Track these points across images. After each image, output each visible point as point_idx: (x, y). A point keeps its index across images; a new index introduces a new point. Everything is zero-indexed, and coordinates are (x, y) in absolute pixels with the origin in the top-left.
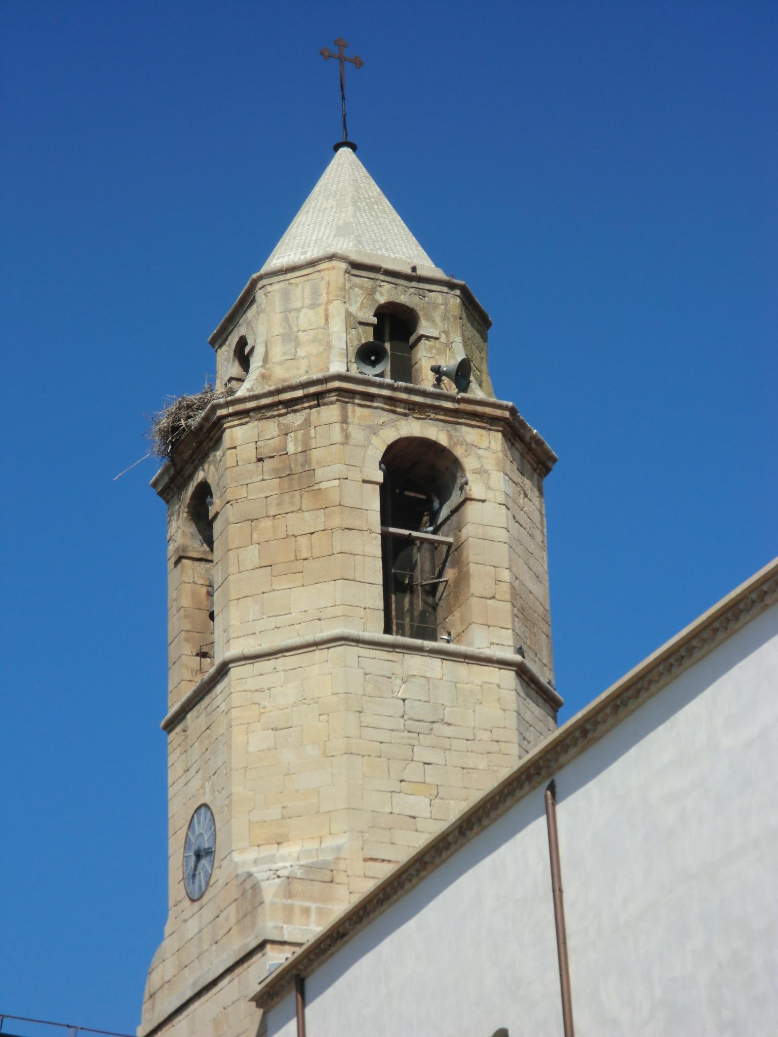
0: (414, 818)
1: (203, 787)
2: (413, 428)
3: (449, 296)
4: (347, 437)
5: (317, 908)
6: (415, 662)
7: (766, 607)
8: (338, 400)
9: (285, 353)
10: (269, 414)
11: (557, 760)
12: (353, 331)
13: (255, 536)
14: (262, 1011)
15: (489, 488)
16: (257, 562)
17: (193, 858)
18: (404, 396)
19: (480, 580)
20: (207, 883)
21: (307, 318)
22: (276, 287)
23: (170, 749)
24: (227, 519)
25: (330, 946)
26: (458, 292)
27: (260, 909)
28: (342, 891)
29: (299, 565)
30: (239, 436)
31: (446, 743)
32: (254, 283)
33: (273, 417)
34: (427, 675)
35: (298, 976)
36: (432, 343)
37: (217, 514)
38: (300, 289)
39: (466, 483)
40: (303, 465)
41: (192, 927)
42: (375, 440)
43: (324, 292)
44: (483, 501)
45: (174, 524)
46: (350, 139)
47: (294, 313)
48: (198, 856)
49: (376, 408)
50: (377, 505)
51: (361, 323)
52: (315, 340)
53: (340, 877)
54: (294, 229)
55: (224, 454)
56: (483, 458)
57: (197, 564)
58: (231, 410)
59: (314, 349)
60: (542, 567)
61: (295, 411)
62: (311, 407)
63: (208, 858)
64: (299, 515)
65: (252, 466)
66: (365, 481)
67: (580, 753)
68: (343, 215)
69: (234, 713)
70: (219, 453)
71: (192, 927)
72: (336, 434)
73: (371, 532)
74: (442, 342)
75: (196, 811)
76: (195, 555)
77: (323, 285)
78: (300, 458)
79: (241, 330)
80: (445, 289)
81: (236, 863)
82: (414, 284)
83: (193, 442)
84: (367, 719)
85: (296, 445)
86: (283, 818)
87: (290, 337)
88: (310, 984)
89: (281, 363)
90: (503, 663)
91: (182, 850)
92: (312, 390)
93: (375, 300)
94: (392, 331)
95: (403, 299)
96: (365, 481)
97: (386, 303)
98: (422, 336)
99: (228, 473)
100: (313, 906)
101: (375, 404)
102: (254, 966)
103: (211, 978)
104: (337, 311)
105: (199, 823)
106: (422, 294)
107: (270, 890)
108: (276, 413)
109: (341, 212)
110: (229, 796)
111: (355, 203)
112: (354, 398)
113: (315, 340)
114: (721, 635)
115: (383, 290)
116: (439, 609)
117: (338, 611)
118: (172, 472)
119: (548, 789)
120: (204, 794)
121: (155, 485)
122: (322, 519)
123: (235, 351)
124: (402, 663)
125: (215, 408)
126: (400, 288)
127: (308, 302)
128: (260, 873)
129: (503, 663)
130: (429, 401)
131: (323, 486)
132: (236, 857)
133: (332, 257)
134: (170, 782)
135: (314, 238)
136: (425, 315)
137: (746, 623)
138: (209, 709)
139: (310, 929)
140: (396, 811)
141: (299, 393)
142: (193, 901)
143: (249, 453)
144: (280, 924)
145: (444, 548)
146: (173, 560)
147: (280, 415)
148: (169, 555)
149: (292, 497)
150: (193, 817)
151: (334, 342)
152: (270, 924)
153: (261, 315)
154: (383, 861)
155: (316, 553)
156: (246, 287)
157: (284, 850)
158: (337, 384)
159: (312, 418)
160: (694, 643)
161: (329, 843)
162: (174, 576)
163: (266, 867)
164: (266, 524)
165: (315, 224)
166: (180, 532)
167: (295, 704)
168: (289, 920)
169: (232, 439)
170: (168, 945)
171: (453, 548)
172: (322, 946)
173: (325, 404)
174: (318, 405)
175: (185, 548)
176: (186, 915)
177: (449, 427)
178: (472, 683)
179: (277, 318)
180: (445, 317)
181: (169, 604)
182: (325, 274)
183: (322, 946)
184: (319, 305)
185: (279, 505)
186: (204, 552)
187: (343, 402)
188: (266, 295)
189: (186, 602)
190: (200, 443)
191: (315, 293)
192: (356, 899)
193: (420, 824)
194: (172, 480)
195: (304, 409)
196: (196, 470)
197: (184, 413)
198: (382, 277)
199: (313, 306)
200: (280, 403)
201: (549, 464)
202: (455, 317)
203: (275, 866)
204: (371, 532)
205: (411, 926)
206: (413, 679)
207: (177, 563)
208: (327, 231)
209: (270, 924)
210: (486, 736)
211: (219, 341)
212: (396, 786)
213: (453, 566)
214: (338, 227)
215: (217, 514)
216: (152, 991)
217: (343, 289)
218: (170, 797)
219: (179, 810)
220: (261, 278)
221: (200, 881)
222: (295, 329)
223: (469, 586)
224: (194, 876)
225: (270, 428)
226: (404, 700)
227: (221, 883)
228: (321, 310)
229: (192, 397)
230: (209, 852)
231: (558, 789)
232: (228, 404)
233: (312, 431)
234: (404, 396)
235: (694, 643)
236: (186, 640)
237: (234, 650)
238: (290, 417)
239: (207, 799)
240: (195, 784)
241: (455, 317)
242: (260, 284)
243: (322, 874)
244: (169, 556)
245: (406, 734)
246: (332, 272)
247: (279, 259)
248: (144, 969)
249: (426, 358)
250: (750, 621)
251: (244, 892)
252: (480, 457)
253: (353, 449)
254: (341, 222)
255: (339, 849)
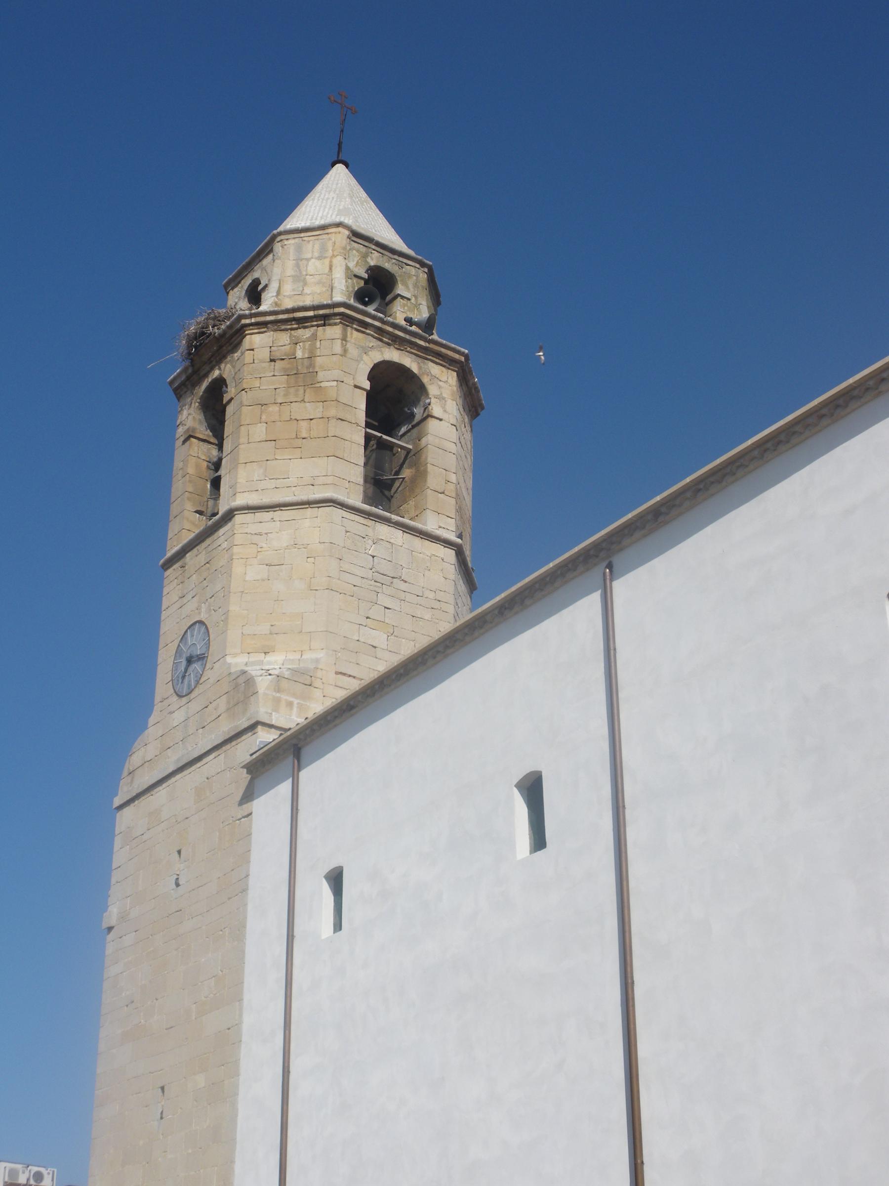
0: (375, 647)
1: (198, 608)
2: (393, 355)
3: (420, 271)
4: (345, 351)
5: (298, 703)
6: (383, 530)
7: (880, 393)
8: (341, 323)
9: (294, 290)
10: (283, 327)
11: (620, 543)
12: (350, 281)
13: (264, 417)
14: (249, 777)
15: (445, 411)
16: (264, 437)
17: (184, 663)
18: (390, 329)
19: (434, 479)
20: (197, 683)
21: (314, 266)
22: (291, 242)
23: (166, 582)
24: (241, 403)
25: (336, 717)
26: (426, 270)
27: (252, 699)
28: (317, 693)
29: (299, 442)
30: (257, 342)
31: (402, 595)
32: (274, 238)
33: (287, 330)
34: (392, 541)
35: (295, 745)
36: (405, 301)
37: (232, 399)
38: (311, 246)
39: (429, 404)
40: (307, 368)
41: (178, 717)
42: (365, 357)
43: (331, 248)
44: (441, 420)
45: (185, 412)
46: (341, 157)
47: (304, 262)
48: (190, 661)
49: (368, 334)
50: (363, 406)
51: (356, 276)
52: (319, 283)
53: (317, 683)
54: (303, 208)
55: (243, 354)
56: (442, 388)
57: (201, 443)
58: (253, 320)
59: (318, 289)
60: (470, 484)
61: (305, 327)
62: (318, 326)
63: (200, 663)
64: (302, 404)
65: (266, 365)
66: (356, 387)
67: (645, 536)
68: (343, 203)
69: (235, 549)
70: (236, 355)
71: (178, 717)
72: (338, 347)
73: (358, 425)
74: (411, 304)
75: (189, 628)
76: (201, 437)
77: (330, 245)
78: (306, 362)
79: (256, 274)
80: (418, 266)
81: (230, 664)
82: (396, 257)
83: (214, 346)
84: (346, 567)
85: (303, 353)
86: (271, 634)
87: (300, 278)
88: (306, 752)
89: (290, 297)
90: (447, 543)
91: (173, 658)
92: (321, 312)
93: (366, 262)
94: (377, 287)
95: (387, 266)
96: (356, 387)
97: (375, 266)
98: (399, 295)
99: (245, 368)
100: (296, 701)
101: (368, 331)
102: (242, 744)
103: (196, 754)
104: (339, 265)
105: (192, 636)
106: (401, 266)
107: (263, 684)
108: (289, 327)
109: (341, 201)
110: (226, 613)
111: (351, 197)
112: (353, 324)
113: (319, 283)
114: (825, 422)
115: (373, 256)
116: (394, 500)
117: (330, 480)
118: (190, 371)
119: (607, 567)
120: (200, 613)
121: (171, 383)
122: (321, 409)
123: (246, 291)
124: (374, 529)
125: (241, 317)
126: (385, 257)
127: (316, 254)
128: (253, 671)
129: (447, 543)
130: (408, 337)
131: (322, 385)
132: (229, 659)
133: (339, 225)
134: (164, 607)
135: (320, 215)
136: (402, 281)
137: (854, 410)
138: (210, 549)
139: (293, 719)
140: (362, 640)
141: (311, 313)
142: (180, 696)
143: (265, 354)
144: (270, 711)
145: (403, 453)
146: (182, 439)
147: (292, 329)
148: (177, 436)
149: (297, 390)
150: (186, 631)
151: (336, 284)
152: (262, 710)
153: (276, 261)
154: (350, 676)
155: (314, 434)
156: (266, 241)
157: (270, 658)
158: (342, 310)
159: (318, 334)
160: (663, 510)
161: (308, 656)
162: (181, 452)
163: (258, 667)
164: (274, 409)
165: (320, 206)
166: (190, 417)
167: (287, 548)
168: (276, 710)
169: (251, 343)
170: (152, 732)
171: (412, 453)
172: (329, 718)
173: (329, 325)
174: (324, 325)
175: (194, 430)
176: (171, 709)
177: (420, 360)
178: (424, 554)
179: (290, 264)
180: (416, 286)
181: (174, 472)
182: (333, 237)
183: (329, 718)
184: (325, 257)
185: (285, 395)
186: (208, 436)
187: (344, 324)
188: (282, 247)
189: (191, 470)
190: (221, 347)
191: (323, 249)
192: (329, 703)
193: (379, 653)
194: (188, 378)
195: (313, 326)
196: (212, 369)
197: (211, 322)
198: (374, 247)
199: (319, 258)
200: (294, 319)
201: (479, 410)
202: (423, 287)
203: (267, 667)
204: (358, 425)
205: (659, 564)
206: (381, 542)
207: (184, 442)
208: (331, 212)
209: (262, 710)
210: (431, 595)
211: (233, 285)
212: (364, 621)
213: (410, 467)
214: (339, 210)
215: (232, 399)
216: (131, 769)
217: (344, 248)
218: (162, 618)
219: (171, 627)
220: (280, 234)
221: (190, 681)
222: (304, 273)
223: (426, 481)
224: (184, 677)
225: (284, 338)
226: (373, 557)
227: (211, 681)
228: (327, 262)
229: (220, 311)
230: (202, 658)
231: (615, 569)
232: (251, 316)
233: (318, 343)
234: (390, 329)
235: (797, 428)
236: (189, 499)
237: (240, 501)
238: (300, 331)
239: (203, 617)
240: (191, 606)
241: (423, 287)
242: (279, 239)
243: (303, 678)
244: (177, 436)
245: (372, 583)
246: (338, 235)
247: (295, 221)
248: (124, 750)
249: (399, 313)
250: (860, 407)
251: (237, 686)
252: (440, 387)
253: (349, 362)
254: (341, 207)
255: (317, 661)
